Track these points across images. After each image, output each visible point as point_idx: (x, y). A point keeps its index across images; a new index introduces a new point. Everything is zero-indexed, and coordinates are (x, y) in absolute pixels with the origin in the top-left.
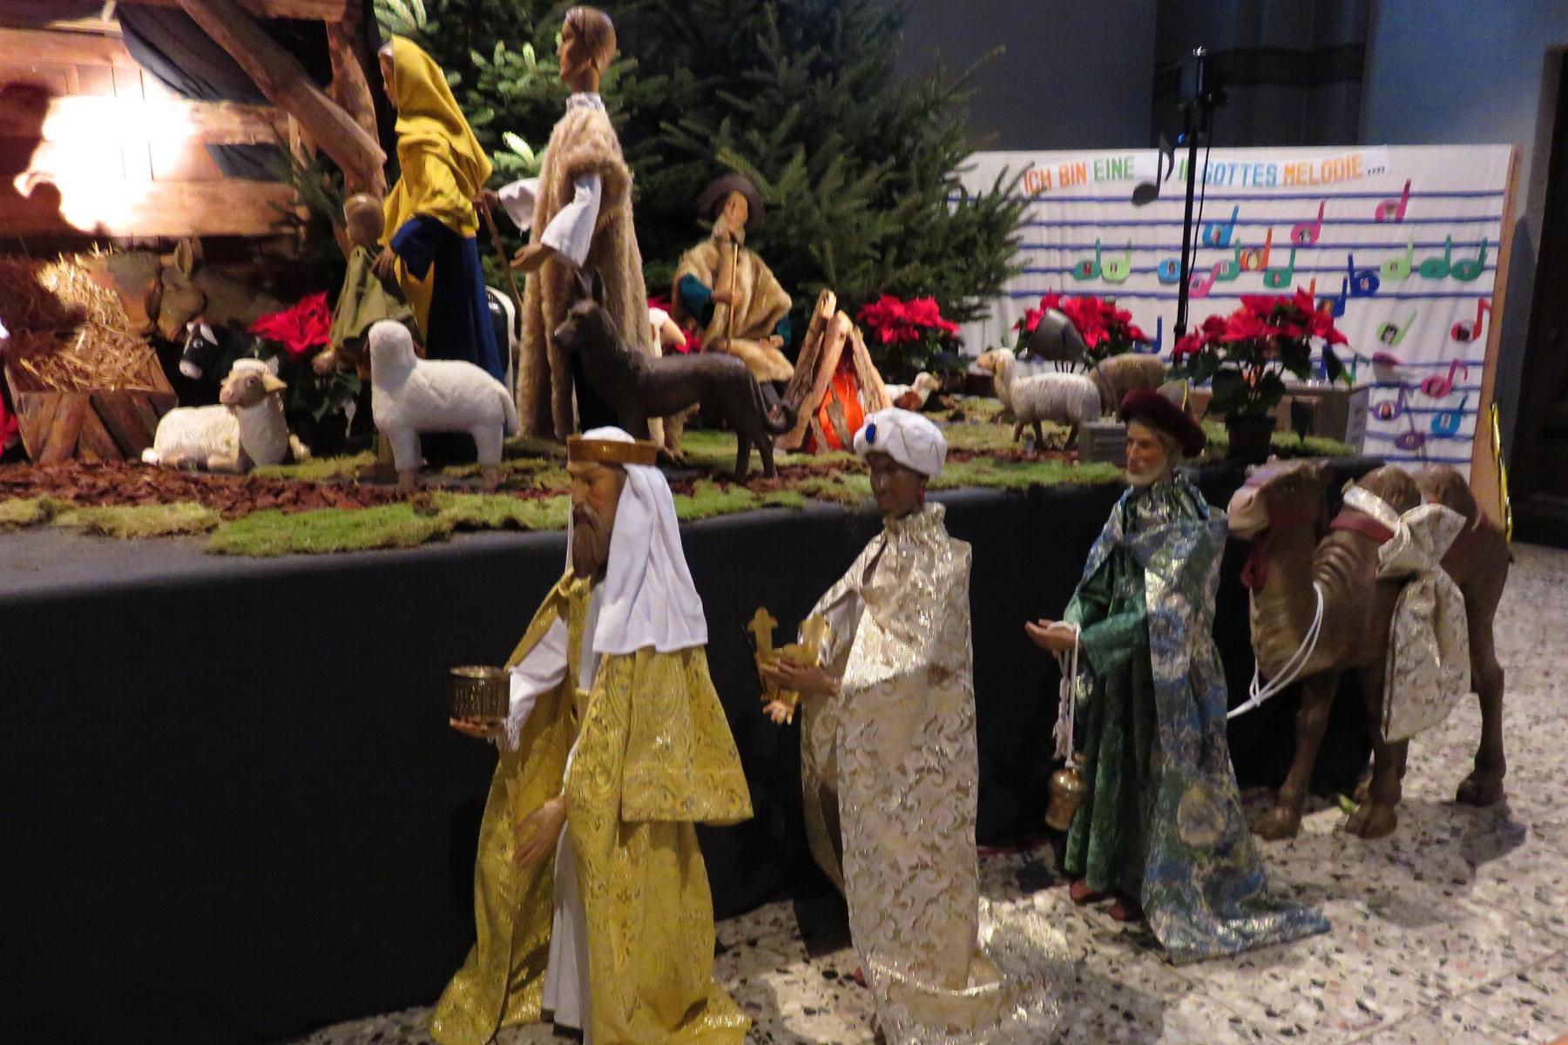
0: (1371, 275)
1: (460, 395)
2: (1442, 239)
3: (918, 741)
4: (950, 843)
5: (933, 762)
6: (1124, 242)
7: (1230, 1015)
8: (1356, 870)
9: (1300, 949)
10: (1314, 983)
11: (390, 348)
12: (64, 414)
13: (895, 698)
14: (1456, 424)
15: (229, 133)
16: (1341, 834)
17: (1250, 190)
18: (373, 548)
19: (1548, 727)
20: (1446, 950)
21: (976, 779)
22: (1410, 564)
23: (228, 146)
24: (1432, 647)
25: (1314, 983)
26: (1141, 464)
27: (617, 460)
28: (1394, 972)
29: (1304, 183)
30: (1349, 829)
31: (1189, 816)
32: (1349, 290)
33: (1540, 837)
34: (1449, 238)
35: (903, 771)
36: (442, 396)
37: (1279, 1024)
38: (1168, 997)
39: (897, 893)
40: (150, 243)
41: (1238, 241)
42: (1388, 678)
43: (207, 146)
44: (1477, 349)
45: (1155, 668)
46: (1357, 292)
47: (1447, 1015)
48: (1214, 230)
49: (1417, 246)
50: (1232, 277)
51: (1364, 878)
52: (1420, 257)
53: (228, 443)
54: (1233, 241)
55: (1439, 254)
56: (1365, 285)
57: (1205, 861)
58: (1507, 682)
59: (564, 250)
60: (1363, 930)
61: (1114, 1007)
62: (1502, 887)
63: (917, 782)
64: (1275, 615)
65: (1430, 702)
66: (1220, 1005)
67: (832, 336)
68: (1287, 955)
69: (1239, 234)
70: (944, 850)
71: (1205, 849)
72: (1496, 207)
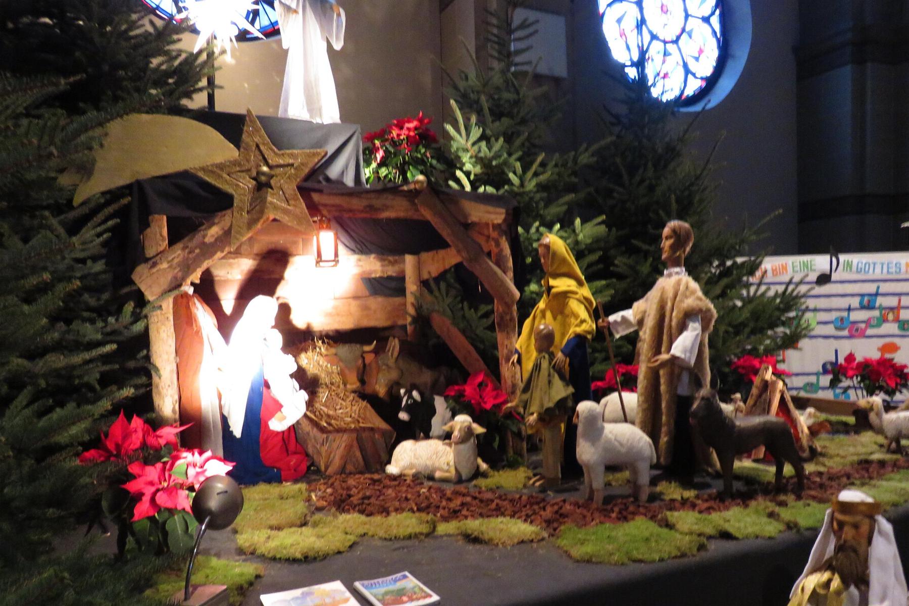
1: (631, 444)
12: (343, 445)
15: (375, 271)
17: (885, 276)
18: (676, 557)
23: (373, 279)
36: (621, 445)
40: (331, 333)
41: (881, 305)
43: (362, 279)
48: (866, 299)
50: (878, 325)
53: (448, 464)
54: (877, 305)
59: (687, 359)
69: (880, 301)
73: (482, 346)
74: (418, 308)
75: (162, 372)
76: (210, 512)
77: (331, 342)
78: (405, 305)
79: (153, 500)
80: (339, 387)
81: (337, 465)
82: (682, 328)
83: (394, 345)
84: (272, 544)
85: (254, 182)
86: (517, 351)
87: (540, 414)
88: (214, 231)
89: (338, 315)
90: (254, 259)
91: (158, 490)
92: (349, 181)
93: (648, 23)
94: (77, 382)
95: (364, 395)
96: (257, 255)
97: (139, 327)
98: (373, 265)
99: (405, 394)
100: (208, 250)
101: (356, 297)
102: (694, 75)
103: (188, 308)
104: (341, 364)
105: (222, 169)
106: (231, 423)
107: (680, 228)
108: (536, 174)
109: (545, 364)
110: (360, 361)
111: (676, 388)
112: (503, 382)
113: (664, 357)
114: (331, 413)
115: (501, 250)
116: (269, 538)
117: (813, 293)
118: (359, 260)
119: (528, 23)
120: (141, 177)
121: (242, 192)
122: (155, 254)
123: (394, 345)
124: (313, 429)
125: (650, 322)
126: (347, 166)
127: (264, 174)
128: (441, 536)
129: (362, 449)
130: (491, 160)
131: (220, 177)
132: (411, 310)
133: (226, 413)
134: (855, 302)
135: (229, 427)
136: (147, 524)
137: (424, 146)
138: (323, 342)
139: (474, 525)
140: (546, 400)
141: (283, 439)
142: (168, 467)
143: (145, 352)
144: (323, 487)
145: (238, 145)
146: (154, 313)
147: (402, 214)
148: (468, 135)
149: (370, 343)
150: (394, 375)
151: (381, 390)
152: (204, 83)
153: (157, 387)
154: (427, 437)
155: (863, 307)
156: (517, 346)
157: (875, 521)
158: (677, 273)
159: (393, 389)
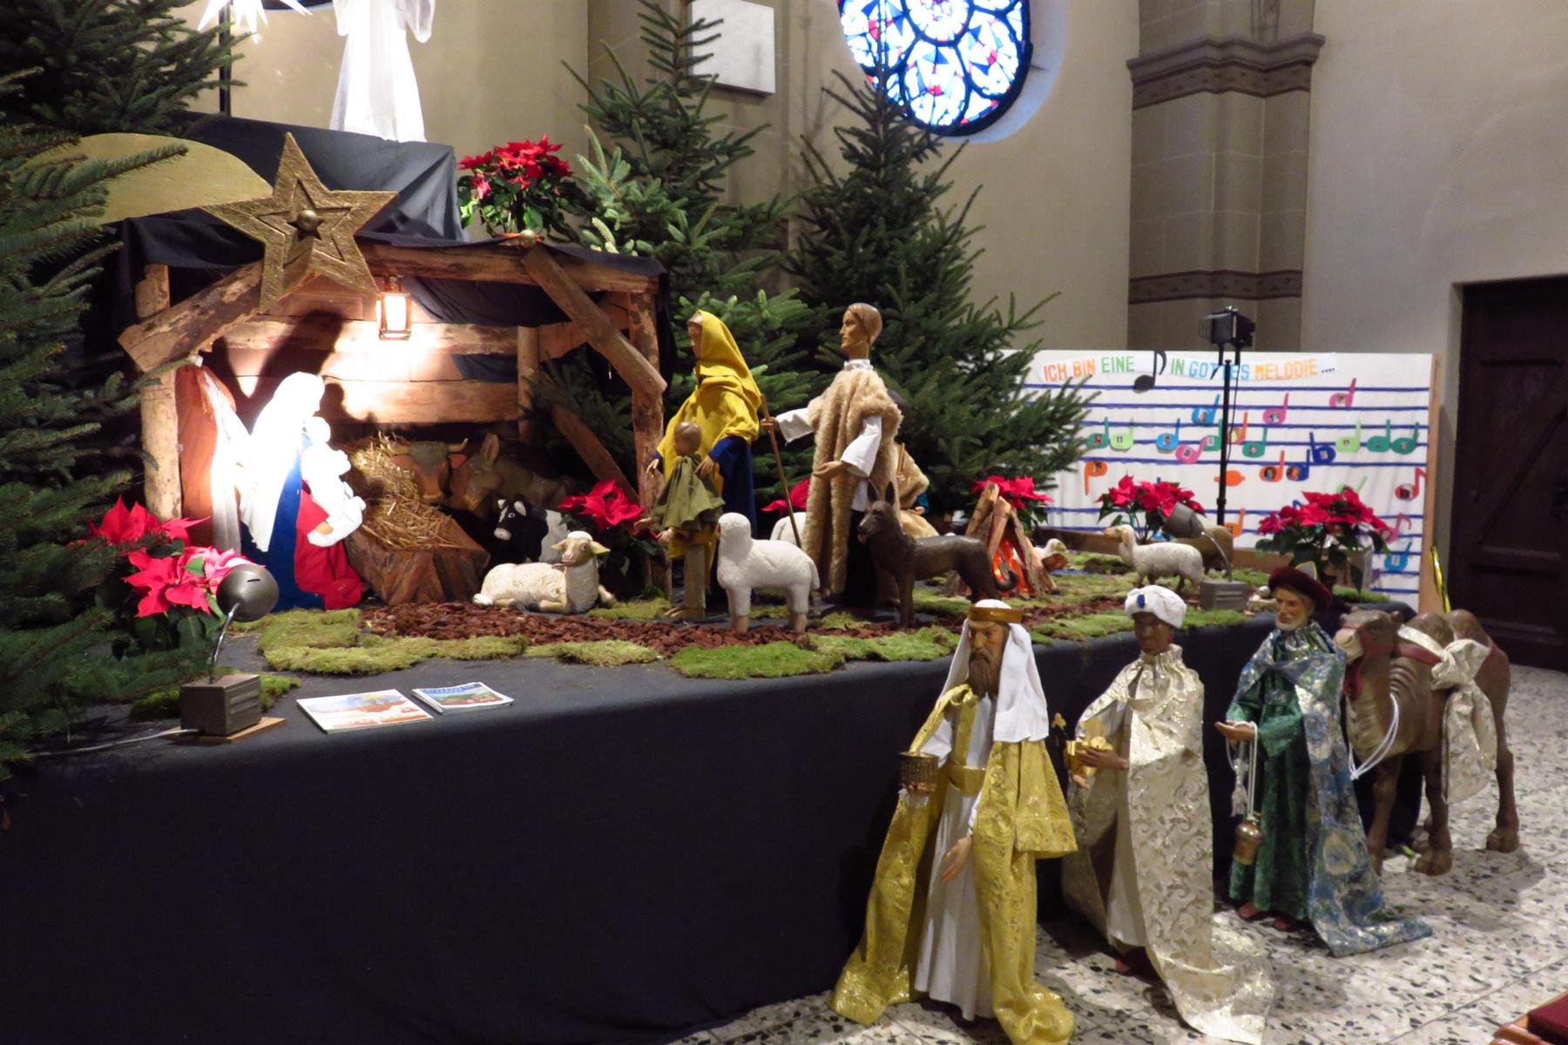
0: (1328, 447)
2: (1383, 422)
3: (1171, 801)
4: (1194, 870)
5: (1181, 815)
6: (1127, 420)
7: (1387, 986)
8: (1433, 896)
9: (1417, 946)
10: (1436, 966)
11: (735, 533)
12: (414, 567)
13: (1163, 772)
14: (1404, 563)
15: (472, 347)
16: (1413, 873)
18: (803, 674)
19: (1535, 797)
20: (1518, 945)
21: (1211, 825)
22: (1455, 679)
24: (1473, 736)
25: (1436, 966)
26: (1289, 616)
27: (1004, 620)
28: (1488, 959)
29: (1271, 379)
30: (1417, 869)
31: (1331, 855)
32: (1311, 460)
33: (1556, 872)
34: (1388, 421)
35: (1162, 820)
37: (1423, 991)
38: (1340, 977)
39: (1161, 904)
40: (404, 428)
42: (1444, 759)
44: (1416, 505)
45: (1311, 752)
46: (1319, 461)
47: (1533, 982)
49: (1364, 427)
51: (1443, 902)
52: (1367, 435)
53: (558, 591)
55: (1382, 433)
56: (1325, 455)
57: (1342, 886)
58: (1516, 762)
60: (1455, 933)
61: (1307, 984)
62: (1540, 905)
63: (1171, 829)
64: (1367, 716)
65: (1474, 775)
66: (1379, 981)
67: (999, 515)
68: (1410, 949)
70: (1190, 875)
71: (1342, 878)
72: (1423, 399)
73: (621, 451)
74: (534, 399)
75: (160, 462)
76: (239, 599)
77: (402, 438)
78: (516, 394)
79: (162, 596)
80: (412, 497)
81: (405, 592)
82: (858, 430)
83: (492, 442)
84: (311, 659)
85: (294, 229)
86: (657, 456)
87: (676, 529)
88: (236, 288)
89: (415, 403)
90: (289, 323)
91: (166, 587)
92: (436, 222)
93: (912, 14)
94: (42, 469)
95: (447, 506)
96: (293, 317)
97: (127, 404)
98: (470, 339)
99: (505, 505)
100: (227, 313)
101: (442, 381)
102: (979, 91)
103: (195, 383)
104: (416, 467)
105: (249, 210)
106: (253, 534)
107: (864, 311)
108: (709, 226)
109: (686, 470)
110: (444, 465)
111: (850, 502)
112: (641, 493)
113: (836, 463)
114: (399, 529)
115: (642, 328)
116: (307, 654)
117: (1097, 400)
118: (449, 330)
119: (705, 23)
120: (133, 215)
121: (277, 240)
122: (151, 313)
123: (492, 442)
124: (371, 546)
125: (824, 424)
126: (432, 202)
127: (308, 219)
128: (531, 658)
129: (441, 574)
130: (644, 205)
131: (246, 219)
132: (525, 402)
133: (246, 522)
134: (1186, 416)
135: (251, 538)
136: (153, 624)
137: (548, 181)
138: (391, 439)
139: (574, 647)
140: (685, 510)
141: (328, 557)
142: (179, 561)
143: (133, 437)
144: (383, 615)
145: (272, 182)
146: (150, 388)
147: (501, 277)
148: (612, 171)
149: (460, 441)
150: (491, 483)
151: (472, 500)
152: (215, 76)
153: (152, 480)
154: (535, 559)
155: (1196, 424)
156: (659, 449)
157: (1009, 628)
158: (858, 366)
159: (489, 499)
